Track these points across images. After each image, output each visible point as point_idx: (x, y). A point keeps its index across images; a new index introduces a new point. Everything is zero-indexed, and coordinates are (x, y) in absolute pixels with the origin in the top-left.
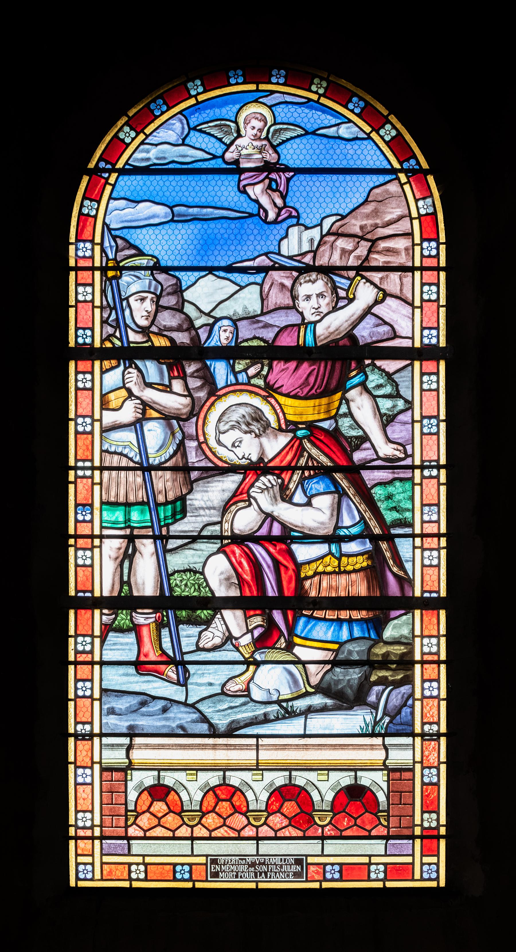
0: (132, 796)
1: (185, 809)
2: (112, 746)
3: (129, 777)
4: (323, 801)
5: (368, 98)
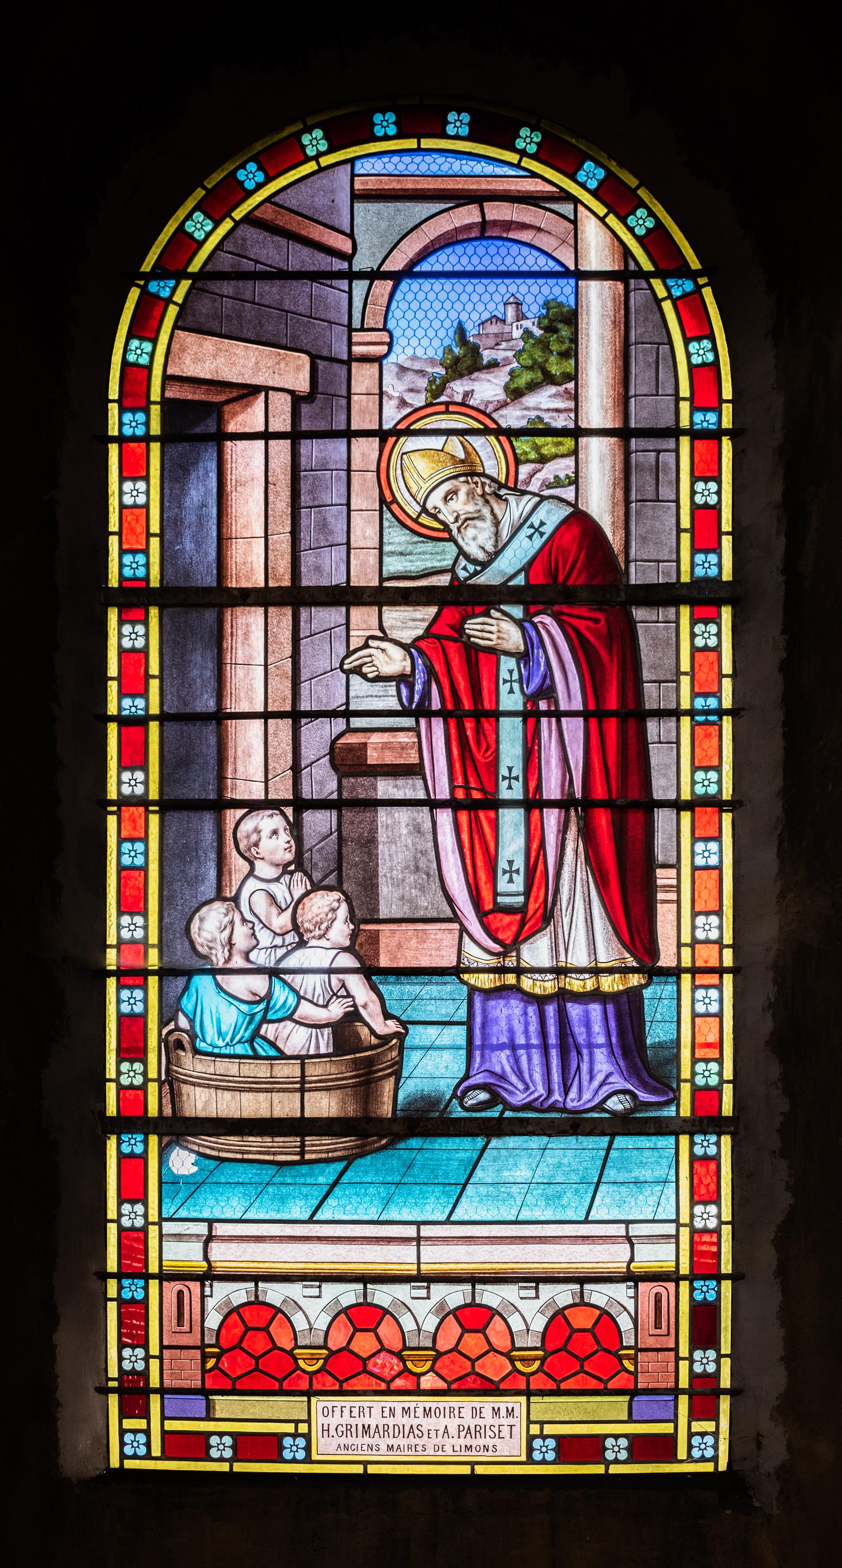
0: (213, 1321)
1: (517, 1345)
2: (179, 1237)
3: (207, 1290)
4: (528, 1330)
5: (613, 166)
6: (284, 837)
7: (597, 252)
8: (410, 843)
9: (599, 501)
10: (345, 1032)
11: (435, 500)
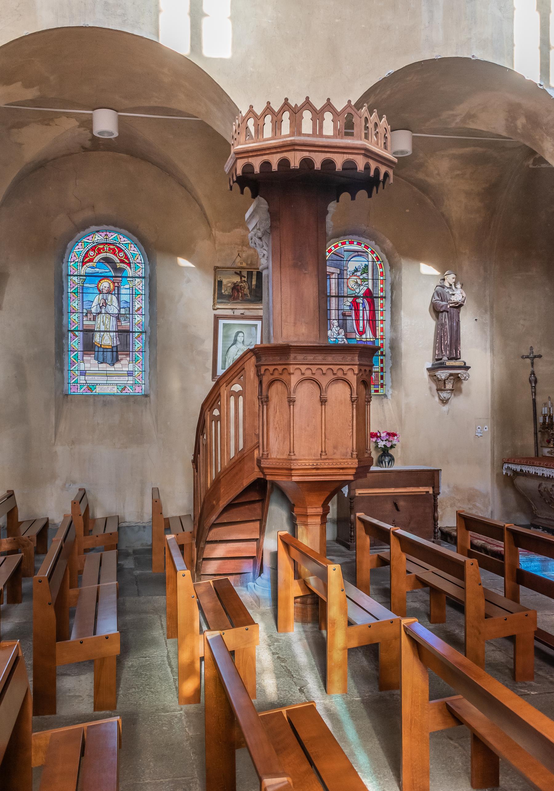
7: (370, 259)
8: (351, 323)
9: (370, 287)
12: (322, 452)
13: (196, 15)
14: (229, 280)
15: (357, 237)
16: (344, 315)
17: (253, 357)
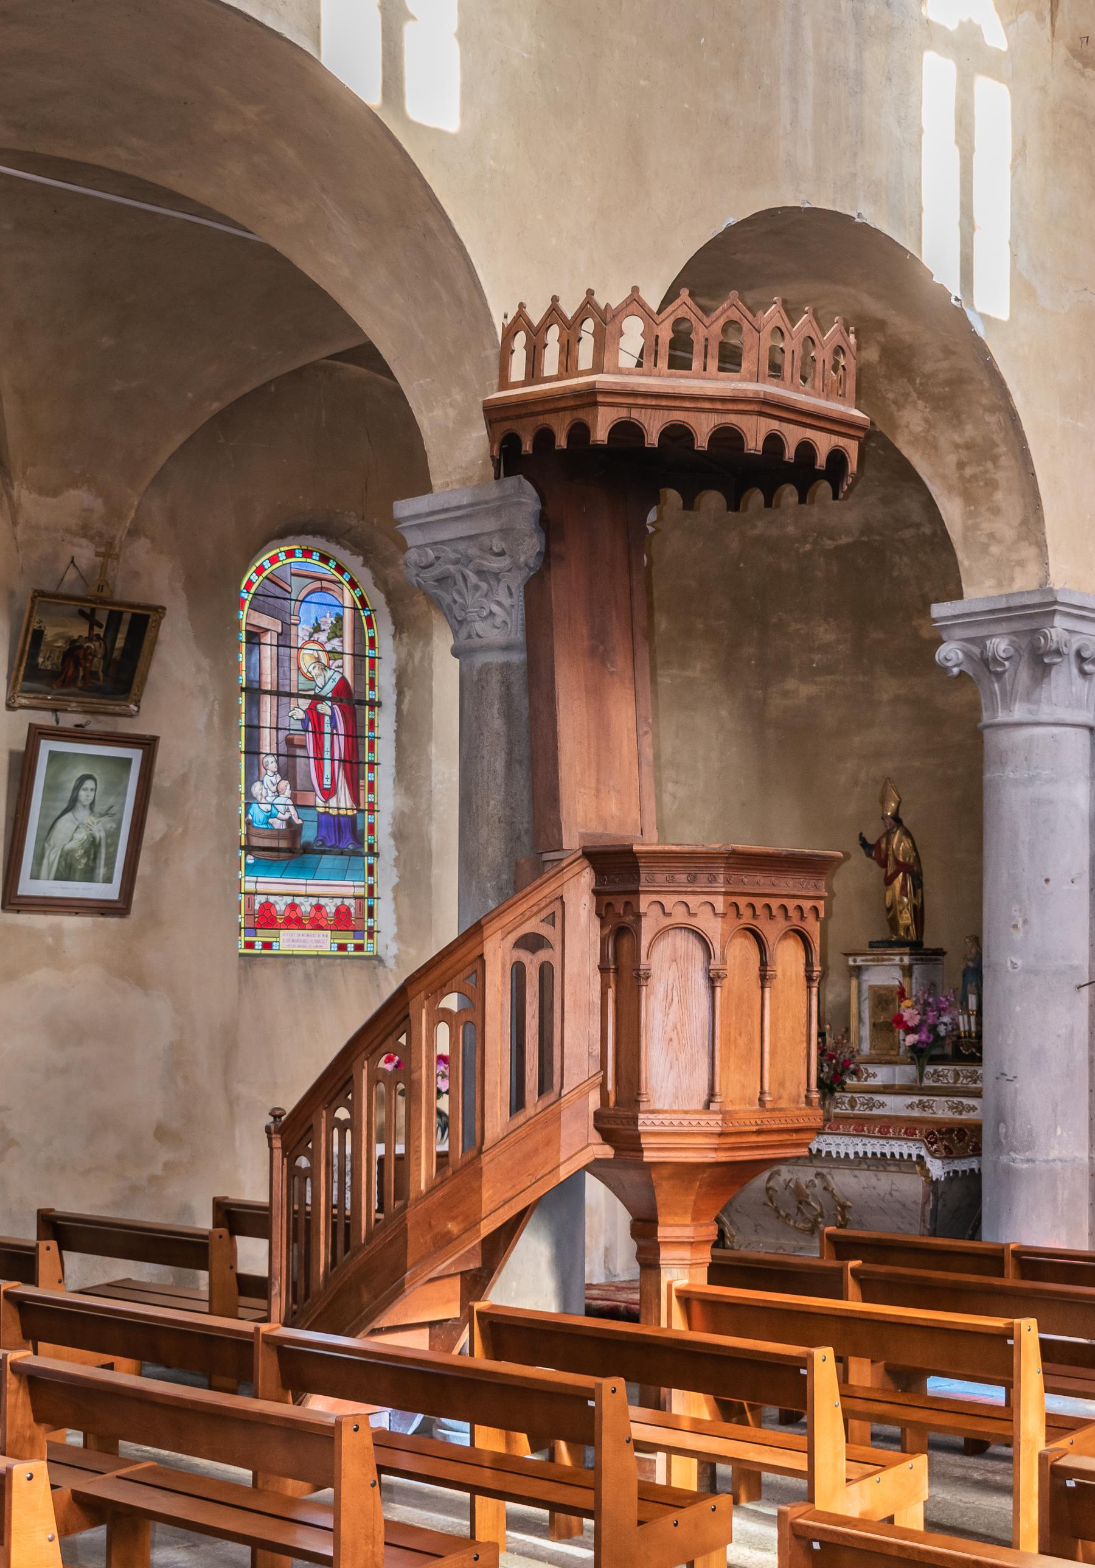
6: (275, 764)
7: (348, 602)
10: (289, 822)
11: (311, 669)
12: (808, 1090)
13: (393, 16)
14: (62, 630)
15: (323, 541)
16: (289, 742)
17: (588, 870)
